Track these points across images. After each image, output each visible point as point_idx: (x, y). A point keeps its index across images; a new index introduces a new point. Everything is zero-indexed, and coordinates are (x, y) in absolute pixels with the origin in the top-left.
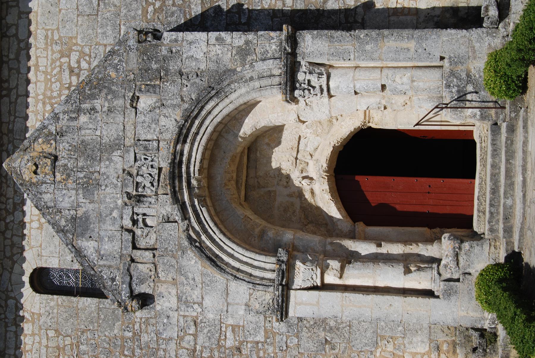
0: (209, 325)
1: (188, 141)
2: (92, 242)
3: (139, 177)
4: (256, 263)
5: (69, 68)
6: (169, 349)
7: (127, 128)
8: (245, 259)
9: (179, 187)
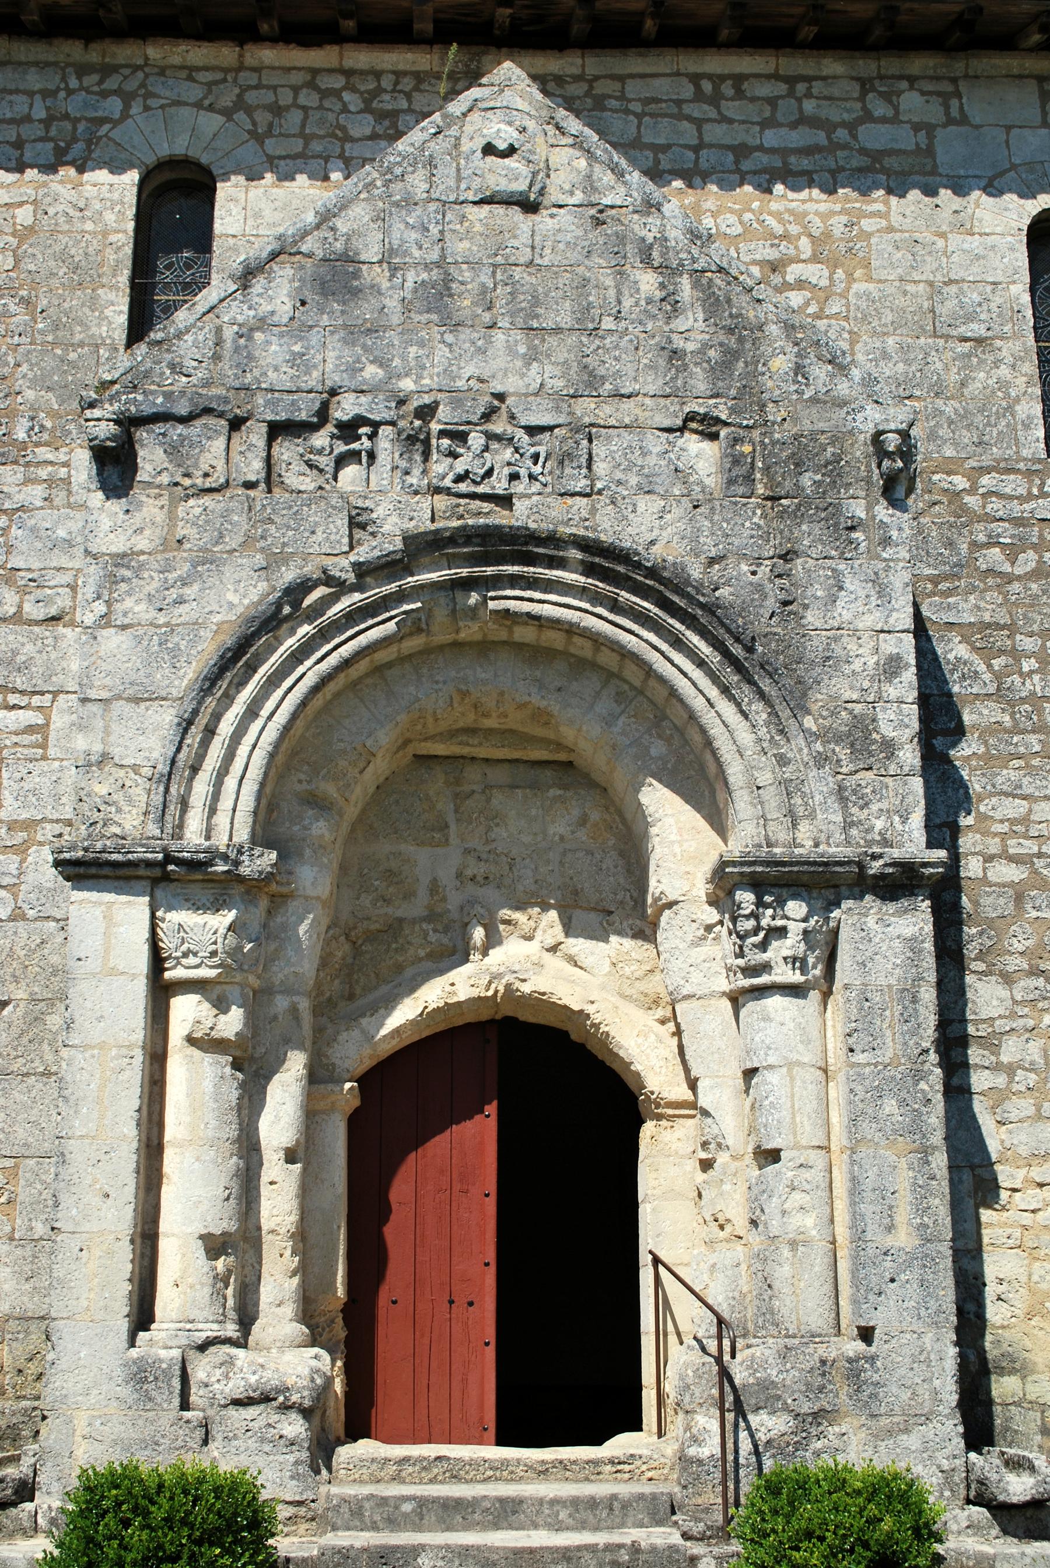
2: (288, 307)
3: (482, 441)
4: (230, 783)
5: (781, 260)
7: (627, 405)
8: (243, 750)
9: (454, 555)
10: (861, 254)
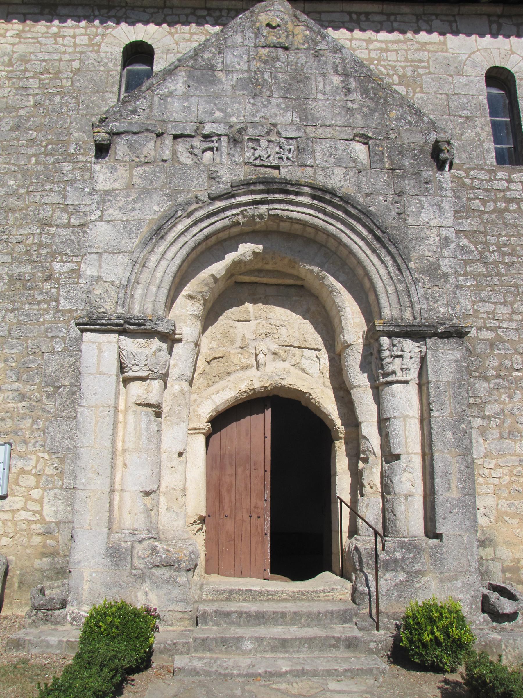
0: (80, 241)
1: (315, 202)
6: (53, 195)
7: (328, 130)
10: (419, 83)
